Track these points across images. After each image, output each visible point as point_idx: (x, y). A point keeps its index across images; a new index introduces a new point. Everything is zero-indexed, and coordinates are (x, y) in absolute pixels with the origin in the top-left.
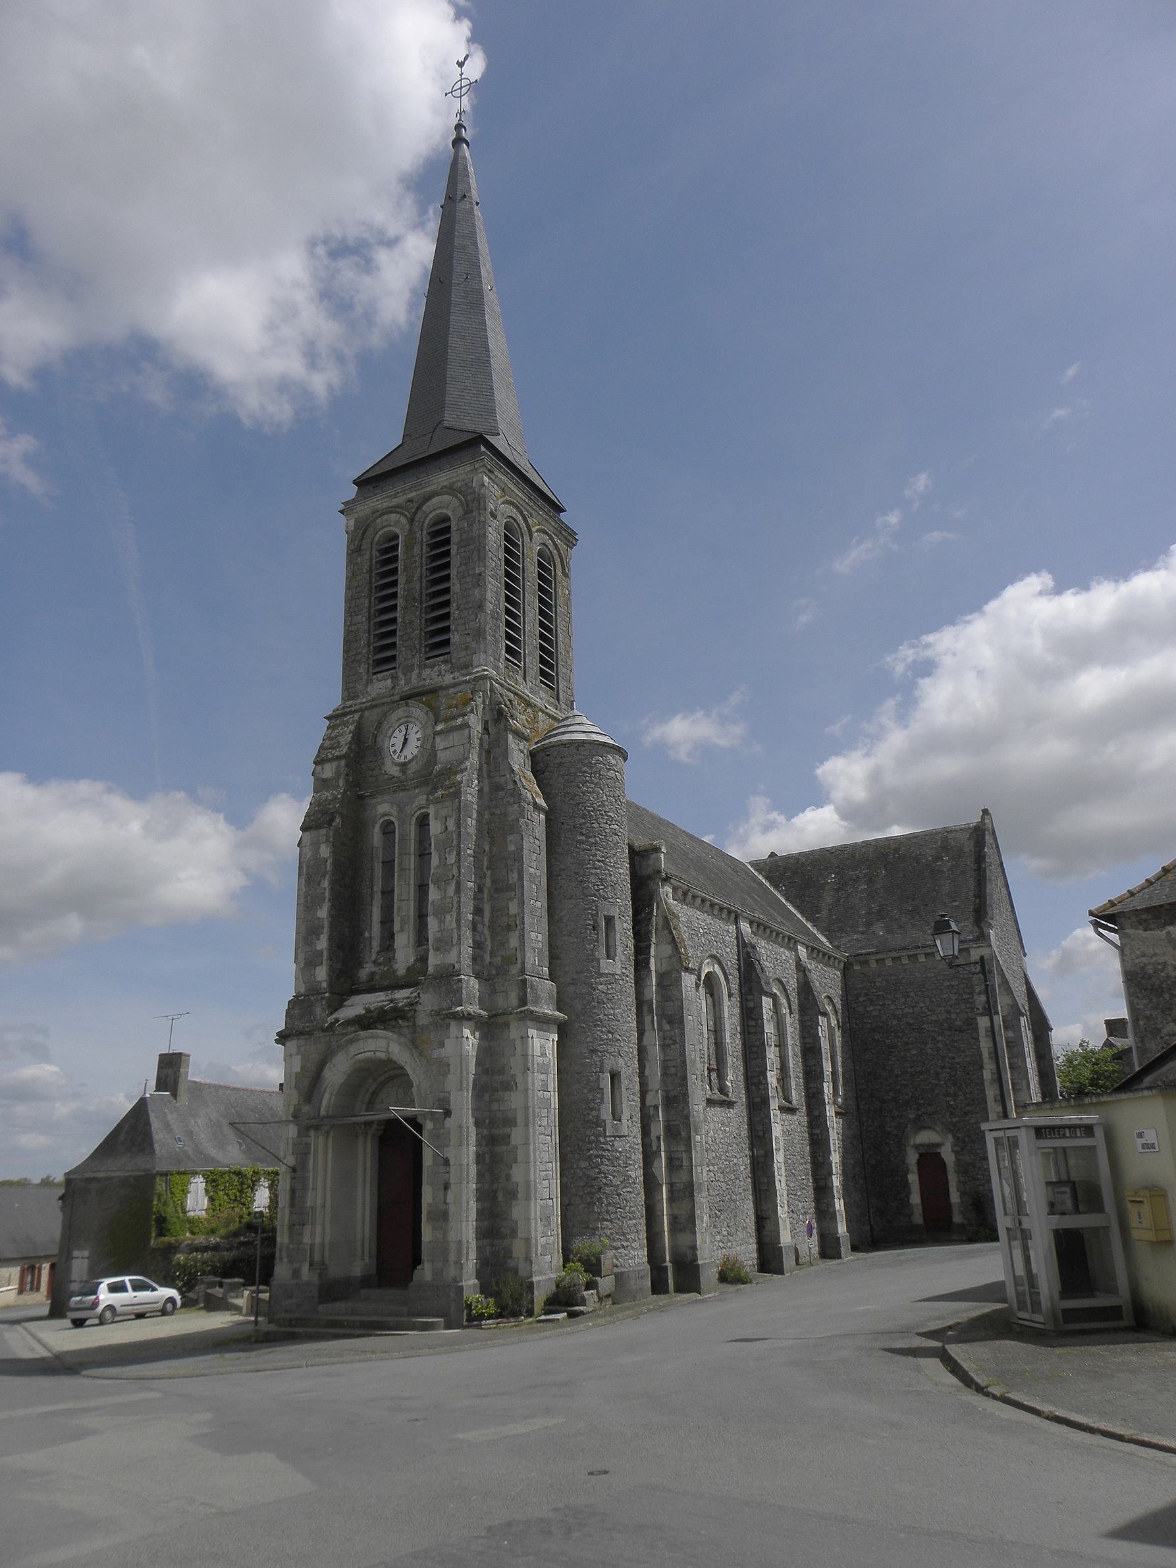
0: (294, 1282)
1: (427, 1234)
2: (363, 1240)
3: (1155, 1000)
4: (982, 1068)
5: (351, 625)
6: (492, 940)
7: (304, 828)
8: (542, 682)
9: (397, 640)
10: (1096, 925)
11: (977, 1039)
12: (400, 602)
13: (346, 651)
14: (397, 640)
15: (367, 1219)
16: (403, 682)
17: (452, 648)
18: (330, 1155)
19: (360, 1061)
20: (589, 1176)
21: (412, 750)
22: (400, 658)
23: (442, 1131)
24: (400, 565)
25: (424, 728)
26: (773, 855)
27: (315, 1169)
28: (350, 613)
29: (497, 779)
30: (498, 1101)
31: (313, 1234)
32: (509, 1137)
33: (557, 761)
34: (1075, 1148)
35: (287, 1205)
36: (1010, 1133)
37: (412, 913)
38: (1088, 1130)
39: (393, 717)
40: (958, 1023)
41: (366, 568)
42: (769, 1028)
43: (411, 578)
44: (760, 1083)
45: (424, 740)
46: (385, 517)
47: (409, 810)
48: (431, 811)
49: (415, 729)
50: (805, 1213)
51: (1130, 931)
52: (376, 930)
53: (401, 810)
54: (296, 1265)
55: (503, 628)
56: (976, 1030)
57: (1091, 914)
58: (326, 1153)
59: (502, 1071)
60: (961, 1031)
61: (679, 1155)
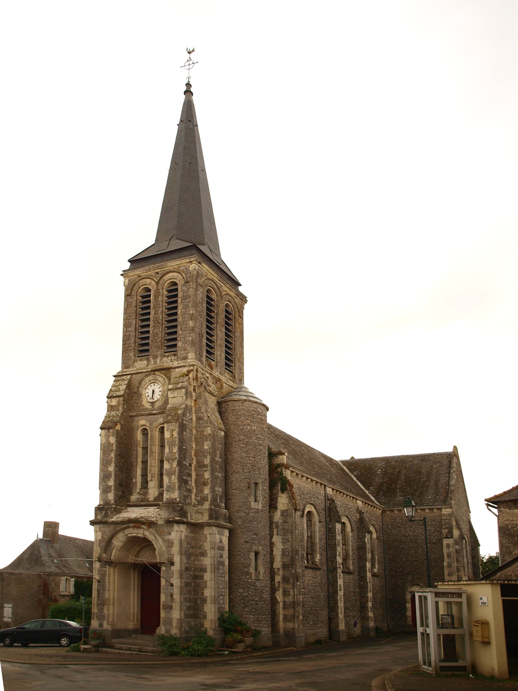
0: (101, 628)
1: (163, 614)
3: (511, 539)
4: (443, 561)
5: (126, 332)
6: (196, 489)
7: (102, 428)
8: (226, 368)
9: (150, 341)
10: (488, 505)
11: (442, 548)
12: (151, 323)
13: (124, 345)
14: (150, 341)
15: (136, 605)
16: (153, 363)
17: (178, 349)
18: (116, 577)
20: (243, 596)
21: (157, 396)
22: (151, 351)
23: (169, 571)
24: (152, 305)
25: (163, 385)
26: (352, 458)
28: (126, 325)
29: (199, 414)
30: (198, 560)
31: (108, 610)
32: (203, 576)
33: (232, 408)
34: (456, 602)
35: (96, 596)
36: (424, 594)
37: (157, 472)
38: (459, 595)
39: (147, 379)
40: (434, 540)
41: (134, 304)
42: (339, 537)
43: (158, 312)
44: (333, 561)
45: (163, 392)
46: (144, 280)
47: (155, 424)
48: (166, 426)
49: (159, 386)
50: (354, 617)
51: (502, 509)
52: (139, 479)
53: (151, 424)
55: (205, 341)
56: (442, 544)
57: (486, 500)
59: (200, 547)
60: (435, 544)
61: (289, 590)
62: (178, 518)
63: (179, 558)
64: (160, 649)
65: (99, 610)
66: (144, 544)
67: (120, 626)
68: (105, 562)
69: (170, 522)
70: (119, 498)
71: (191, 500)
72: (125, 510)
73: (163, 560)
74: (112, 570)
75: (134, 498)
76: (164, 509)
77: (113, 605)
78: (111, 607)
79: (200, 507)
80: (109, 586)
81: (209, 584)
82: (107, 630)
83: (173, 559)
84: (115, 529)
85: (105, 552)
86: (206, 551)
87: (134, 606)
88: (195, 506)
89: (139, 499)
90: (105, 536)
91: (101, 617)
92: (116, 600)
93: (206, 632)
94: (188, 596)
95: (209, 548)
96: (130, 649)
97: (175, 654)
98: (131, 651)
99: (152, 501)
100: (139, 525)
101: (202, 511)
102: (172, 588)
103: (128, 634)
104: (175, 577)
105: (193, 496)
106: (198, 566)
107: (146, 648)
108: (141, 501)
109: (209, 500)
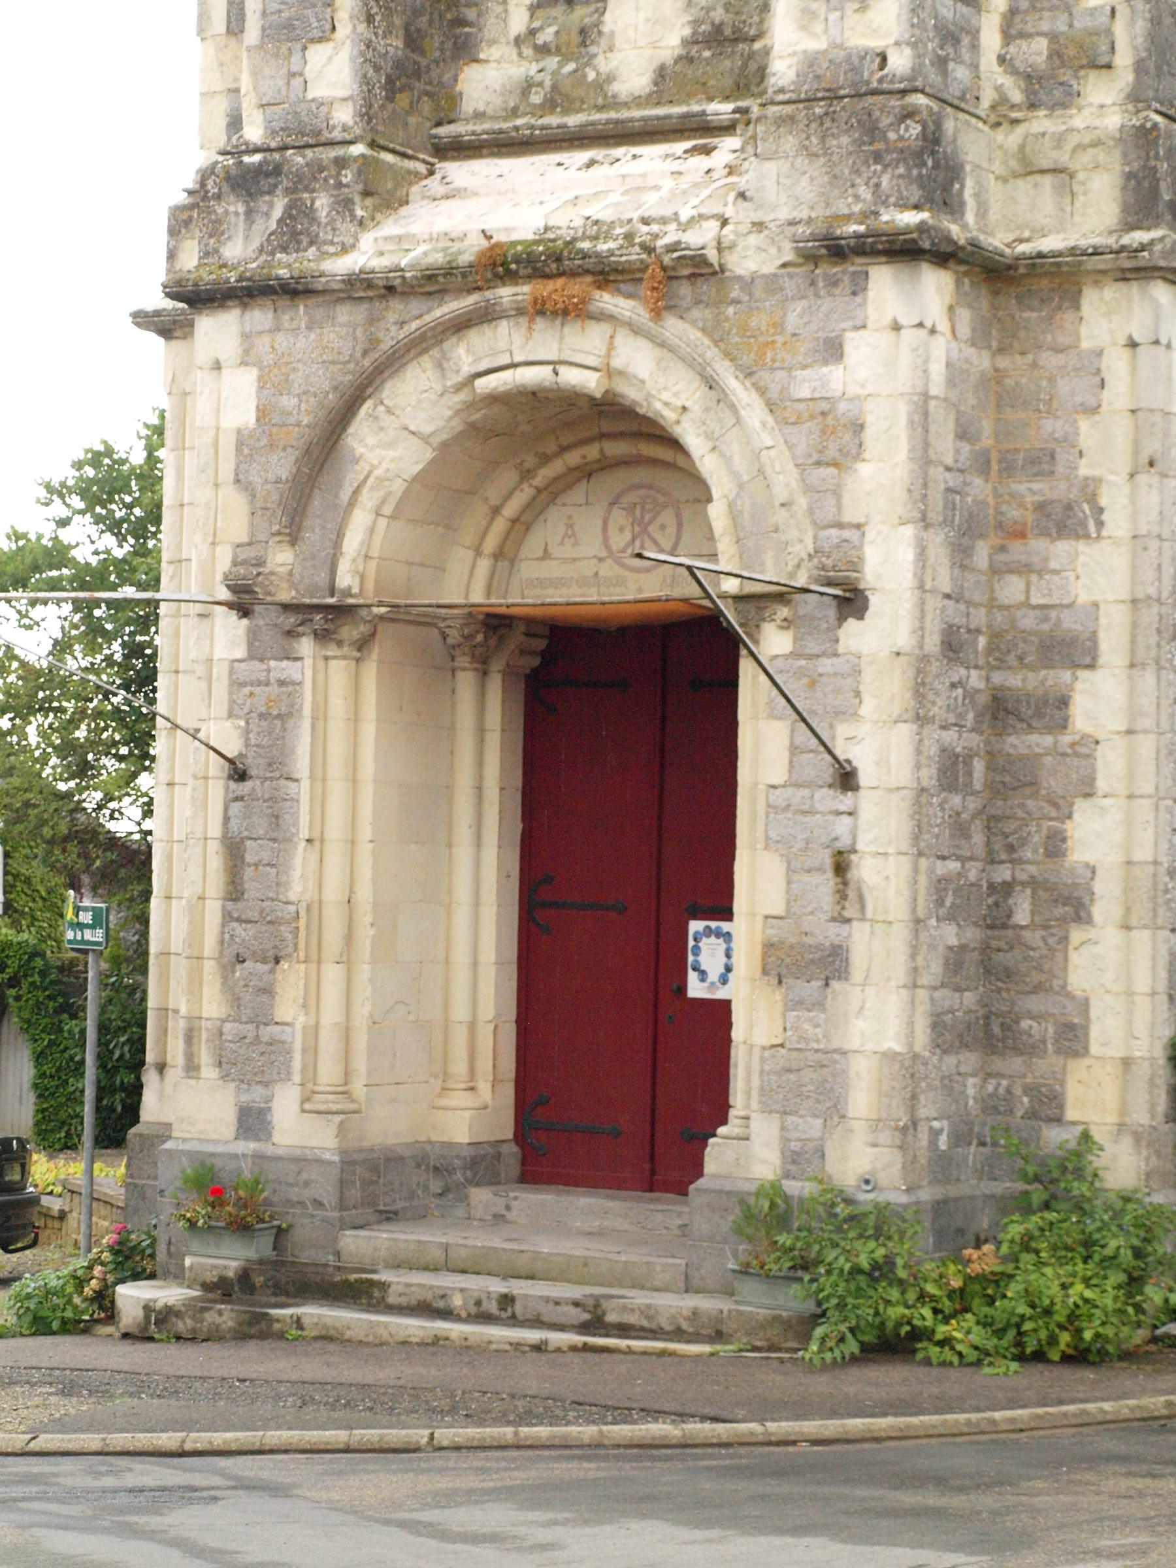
0: (251, 1146)
2: (472, 1026)
18: (369, 731)
19: (494, 399)
23: (826, 665)
27: (319, 776)
30: (1025, 569)
31: (311, 1001)
32: (1064, 702)
54: (256, 1094)
58: (355, 719)
59: (1042, 462)
62: (910, 218)
63: (907, 555)
64: (758, 1302)
65: (236, 1001)
66: (573, 458)
67: (390, 1125)
68: (286, 607)
69: (838, 253)
70: (392, 89)
71: (975, 67)
72: (433, 183)
73: (770, 572)
74: (339, 671)
75: (488, 82)
76: (790, 142)
77: (347, 960)
78: (332, 974)
79: (1041, 123)
80: (320, 803)
81: (1110, 766)
82: (301, 1161)
83: (856, 565)
84: (374, 342)
85: (293, 534)
86: (1090, 490)
87: (475, 964)
88: (1002, 116)
89: (528, 86)
90: (288, 402)
91: (252, 1055)
92: (364, 917)
93: (1076, 1161)
94: (953, 866)
95: (1124, 464)
96: (505, 1310)
97: (893, 1345)
98: (514, 1321)
99: (638, 101)
100: (577, 287)
101: (1063, 158)
102: (846, 801)
103: (436, 1186)
104: (868, 708)
105: (991, 39)
106: (1028, 621)
107: (640, 1298)
108: (550, 105)
109: (1124, 59)
